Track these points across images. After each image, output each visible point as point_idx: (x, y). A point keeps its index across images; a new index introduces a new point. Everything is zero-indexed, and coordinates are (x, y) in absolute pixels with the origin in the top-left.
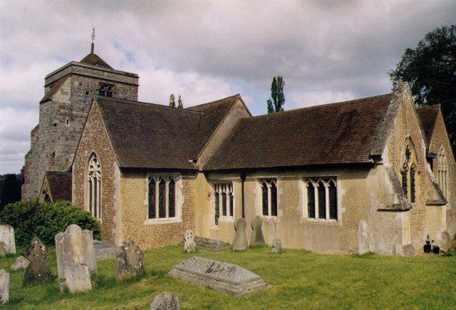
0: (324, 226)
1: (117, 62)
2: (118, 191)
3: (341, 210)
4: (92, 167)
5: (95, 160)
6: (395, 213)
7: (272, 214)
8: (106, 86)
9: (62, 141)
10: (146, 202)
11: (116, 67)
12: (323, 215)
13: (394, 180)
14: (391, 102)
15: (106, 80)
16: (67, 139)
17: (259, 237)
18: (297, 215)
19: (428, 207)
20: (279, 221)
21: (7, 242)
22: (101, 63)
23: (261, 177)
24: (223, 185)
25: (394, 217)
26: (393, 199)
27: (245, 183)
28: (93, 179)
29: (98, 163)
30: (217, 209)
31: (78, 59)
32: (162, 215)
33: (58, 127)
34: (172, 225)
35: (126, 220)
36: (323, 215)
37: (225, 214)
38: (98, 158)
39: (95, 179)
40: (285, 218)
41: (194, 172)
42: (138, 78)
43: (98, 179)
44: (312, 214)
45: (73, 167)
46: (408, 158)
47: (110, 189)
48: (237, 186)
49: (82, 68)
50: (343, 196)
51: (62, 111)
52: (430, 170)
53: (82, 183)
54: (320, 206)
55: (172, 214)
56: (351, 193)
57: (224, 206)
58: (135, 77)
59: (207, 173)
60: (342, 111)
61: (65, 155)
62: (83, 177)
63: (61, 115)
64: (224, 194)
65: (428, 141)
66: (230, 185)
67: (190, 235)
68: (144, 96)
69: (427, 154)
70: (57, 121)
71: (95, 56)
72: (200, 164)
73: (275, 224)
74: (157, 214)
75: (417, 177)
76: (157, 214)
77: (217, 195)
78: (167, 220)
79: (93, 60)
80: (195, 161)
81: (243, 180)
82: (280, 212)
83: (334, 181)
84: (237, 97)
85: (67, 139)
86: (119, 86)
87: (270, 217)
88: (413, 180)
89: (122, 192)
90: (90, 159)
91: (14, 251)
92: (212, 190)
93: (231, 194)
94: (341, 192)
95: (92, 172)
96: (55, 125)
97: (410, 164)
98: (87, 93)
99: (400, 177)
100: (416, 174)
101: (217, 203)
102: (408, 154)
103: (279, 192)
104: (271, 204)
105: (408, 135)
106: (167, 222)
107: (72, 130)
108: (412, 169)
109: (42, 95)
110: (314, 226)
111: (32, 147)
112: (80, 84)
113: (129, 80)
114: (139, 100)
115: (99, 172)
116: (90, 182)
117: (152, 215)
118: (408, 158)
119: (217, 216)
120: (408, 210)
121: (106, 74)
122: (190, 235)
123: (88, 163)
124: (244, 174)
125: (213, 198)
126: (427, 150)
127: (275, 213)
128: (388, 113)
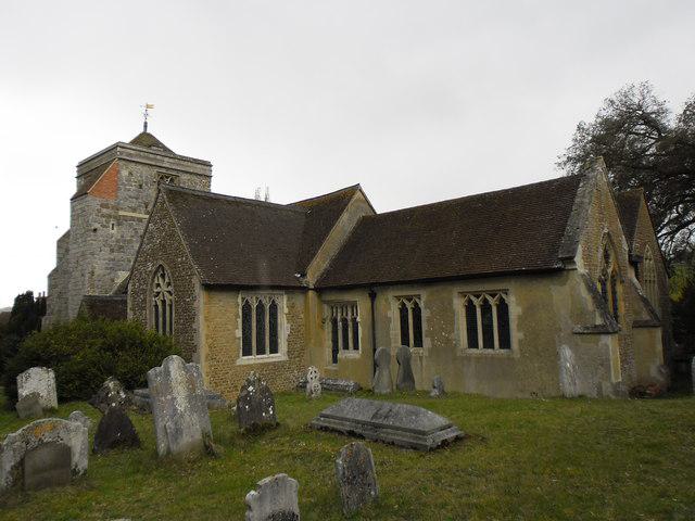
0: (492, 358)
1: (180, 143)
2: (201, 318)
3: (516, 335)
4: (158, 285)
5: (163, 276)
6: (597, 337)
7: (501, 347)
8: (167, 177)
9: (106, 253)
10: (239, 333)
11: (179, 151)
12: (489, 344)
13: (591, 289)
14: (581, 184)
15: (167, 169)
16: (112, 251)
17: (408, 376)
18: (450, 345)
19: (636, 331)
20: (426, 354)
21: (44, 394)
22: (157, 143)
23: (405, 293)
24: (344, 306)
25: (598, 341)
26: (594, 318)
27: (377, 302)
28: (159, 303)
29: (167, 280)
30: (335, 341)
31: (127, 138)
32: (261, 351)
33: (99, 233)
34: (274, 364)
35: (211, 358)
36: (489, 344)
37: (346, 347)
38: (168, 272)
39: (164, 302)
40: (434, 350)
41: (304, 290)
42: (211, 166)
43: (168, 302)
44: (473, 343)
45: (130, 287)
46: (607, 262)
47: (188, 316)
48: (362, 303)
49: (132, 152)
50: (520, 318)
51: (104, 210)
52: (635, 280)
53: (144, 308)
54: (250, 329)
55: (274, 350)
56: (529, 311)
57: (344, 334)
58: (208, 165)
59: (320, 290)
60: (444, 206)
62: (144, 300)
63: (103, 216)
64: (345, 321)
65: (630, 236)
66: (354, 305)
67: (314, 375)
68: (219, 186)
69: (630, 256)
70: (97, 226)
71: (149, 134)
72: (311, 279)
73: (421, 358)
74: (268, 349)
75: (620, 289)
76: (268, 349)
77: (335, 322)
78: (268, 358)
79: (146, 141)
80: (304, 275)
81: (373, 296)
82: (427, 342)
83: (504, 296)
84: (356, 188)
85: (112, 251)
86: (184, 177)
87: (497, 351)
88: (614, 293)
89: (206, 319)
90: (155, 273)
91: (54, 403)
92: (327, 312)
93: (354, 320)
94: (515, 311)
95: (158, 293)
96: (95, 230)
97: (610, 271)
98: (141, 186)
99: (599, 286)
100: (618, 283)
101: (335, 332)
102: (606, 256)
103: (425, 314)
104: (412, 329)
105: (606, 231)
106: (266, 361)
108: (613, 277)
109: (73, 190)
110: (479, 359)
111: (58, 262)
112: (131, 173)
113: (199, 169)
114: (212, 191)
115: (169, 292)
116: (156, 306)
117: (247, 352)
118: (607, 262)
119: (335, 351)
120: (616, 332)
121: (166, 159)
122: (314, 375)
123: (153, 281)
124: (373, 290)
125: (328, 327)
126: (630, 251)
127: (419, 343)
128: (577, 200)
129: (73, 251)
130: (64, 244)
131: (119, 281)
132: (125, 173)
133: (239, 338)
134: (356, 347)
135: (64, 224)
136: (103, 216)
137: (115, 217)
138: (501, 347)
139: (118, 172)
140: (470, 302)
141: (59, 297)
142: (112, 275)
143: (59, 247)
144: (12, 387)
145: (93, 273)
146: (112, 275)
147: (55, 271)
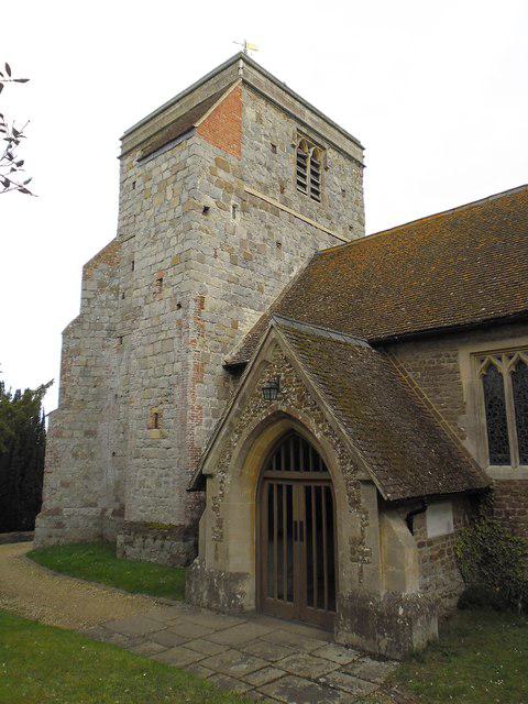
9: (222, 263)
16: (234, 262)
33: (213, 215)
42: (362, 166)
51: (221, 173)
61: (231, 309)
63: (220, 184)
70: (211, 203)
86: (331, 153)
96: (206, 210)
107: (245, 236)
111: (83, 307)
129: (143, 263)
130: (104, 271)
131: (246, 328)
132: (250, 113)
133: (239, 577)
134: (290, 598)
135: (73, 310)
136: (220, 184)
137: (237, 192)
138: (288, 600)
139: (240, 110)
140: (491, 366)
141: (84, 374)
142: (234, 314)
143: (85, 278)
144: (72, 345)
145: (201, 302)
146: (234, 314)
147: (78, 322)
